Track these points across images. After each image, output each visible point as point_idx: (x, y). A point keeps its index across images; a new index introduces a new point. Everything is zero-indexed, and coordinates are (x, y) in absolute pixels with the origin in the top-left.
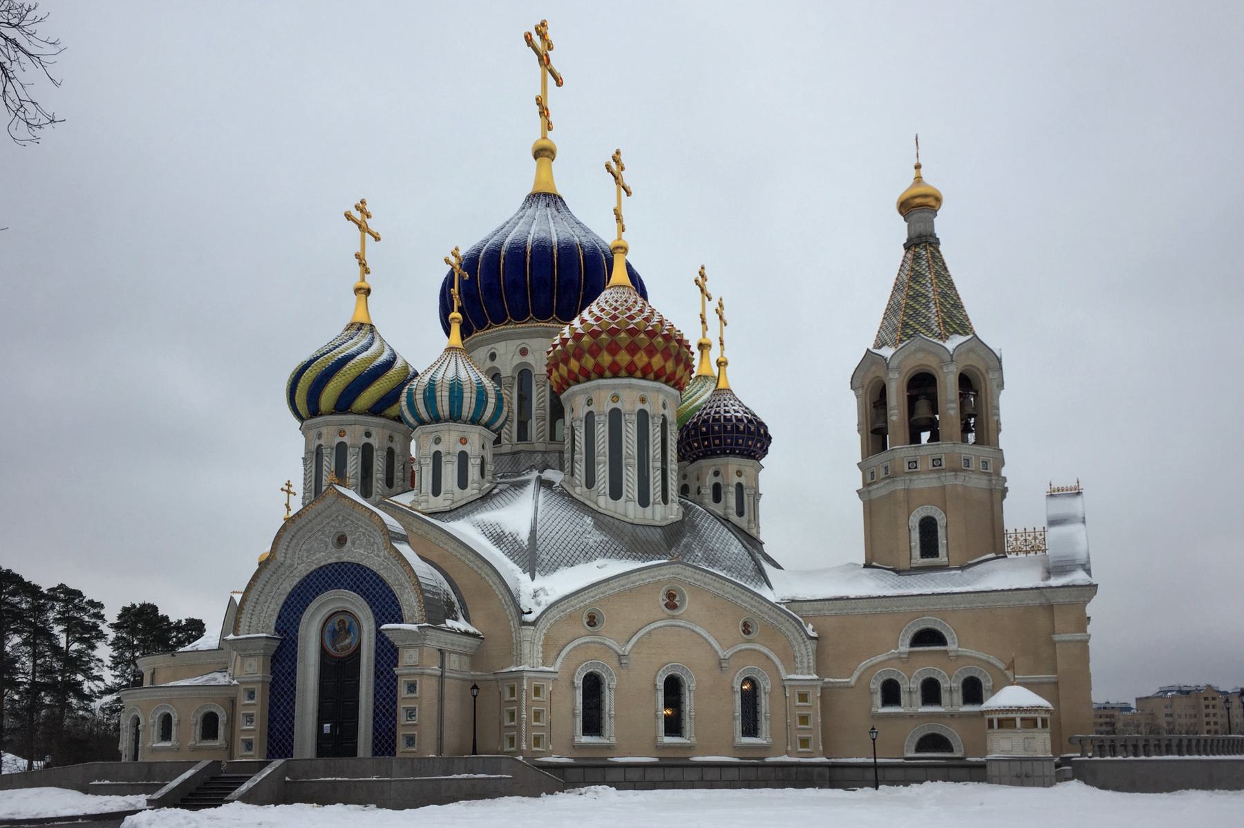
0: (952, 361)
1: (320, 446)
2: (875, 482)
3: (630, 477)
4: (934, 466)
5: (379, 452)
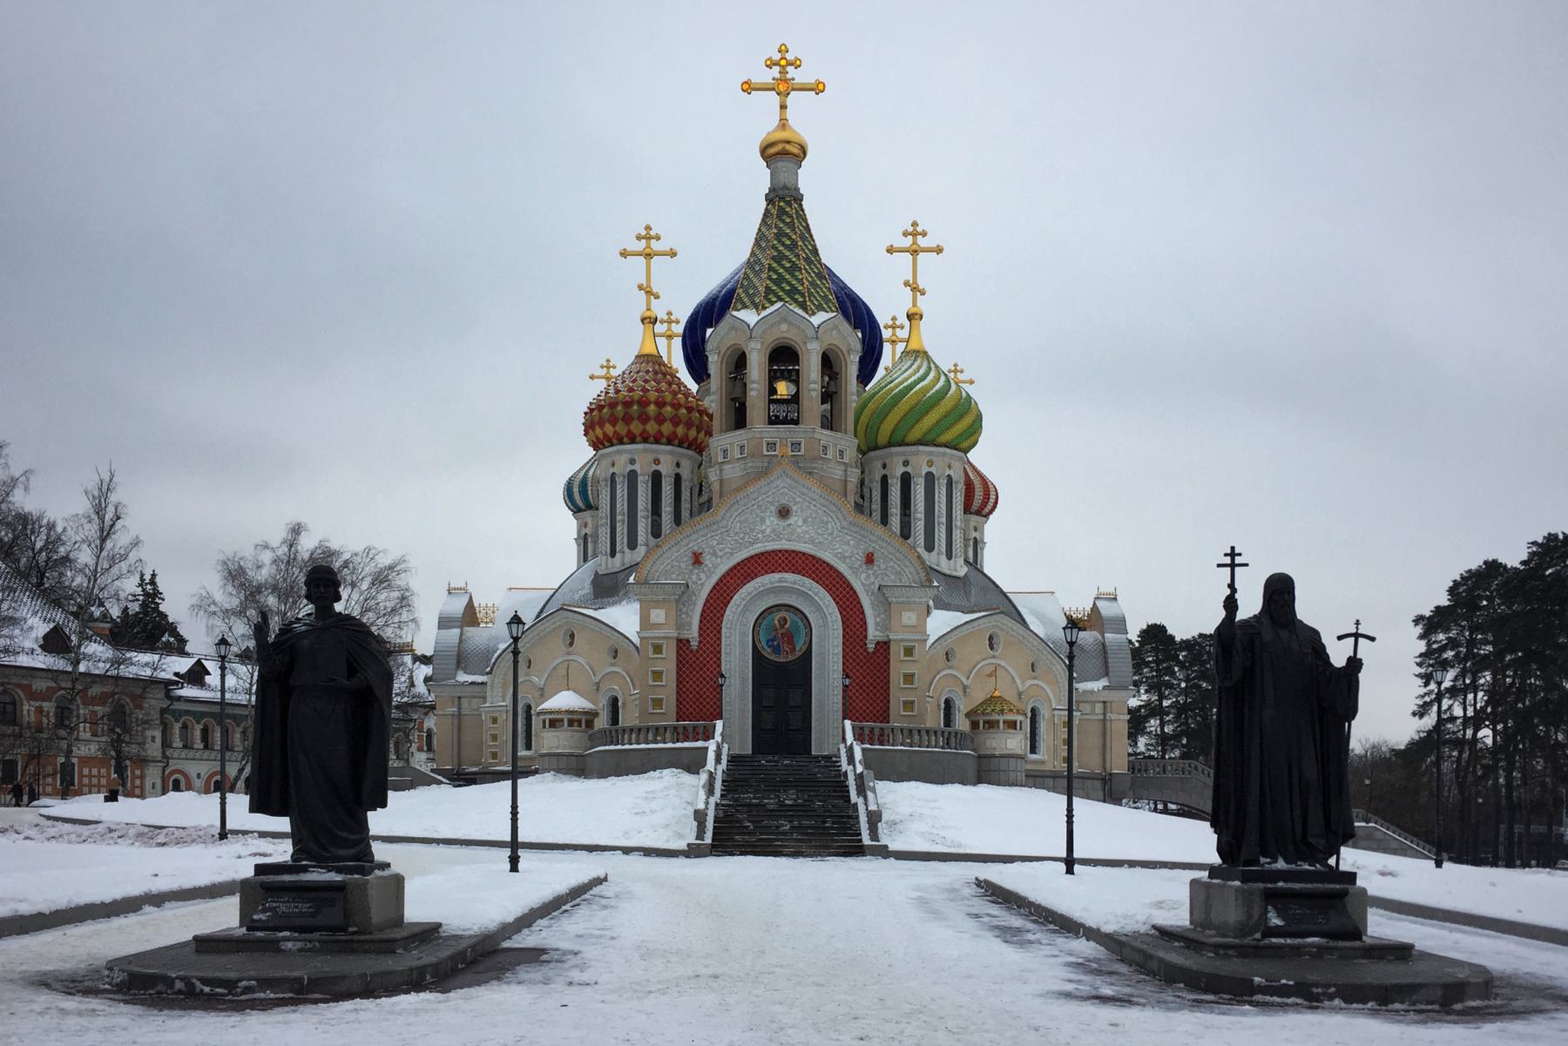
0: (817, 338)
1: (614, 474)
2: (729, 461)
3: (919, 527)
4: (792, 451)
5: (668, 479)
